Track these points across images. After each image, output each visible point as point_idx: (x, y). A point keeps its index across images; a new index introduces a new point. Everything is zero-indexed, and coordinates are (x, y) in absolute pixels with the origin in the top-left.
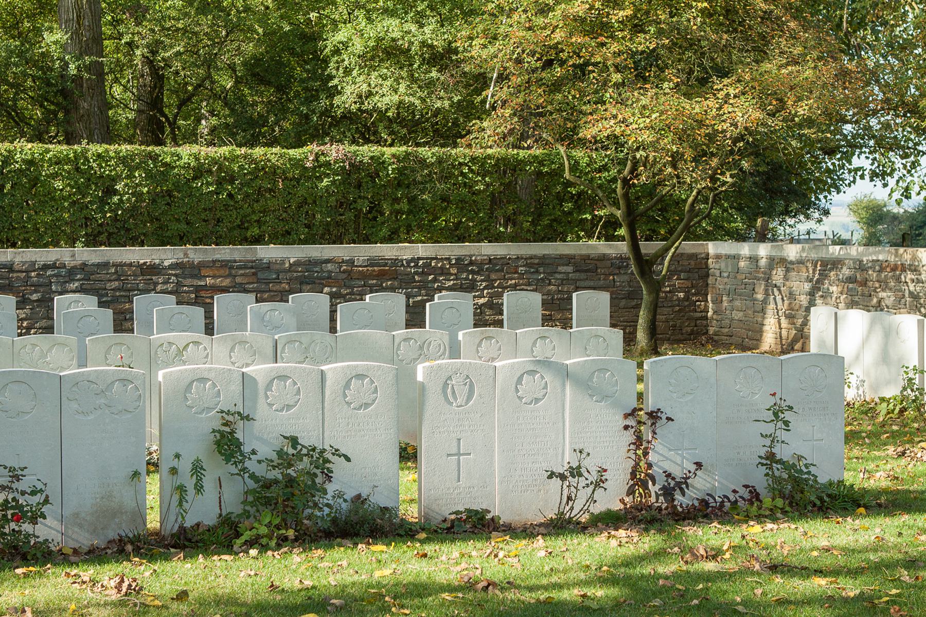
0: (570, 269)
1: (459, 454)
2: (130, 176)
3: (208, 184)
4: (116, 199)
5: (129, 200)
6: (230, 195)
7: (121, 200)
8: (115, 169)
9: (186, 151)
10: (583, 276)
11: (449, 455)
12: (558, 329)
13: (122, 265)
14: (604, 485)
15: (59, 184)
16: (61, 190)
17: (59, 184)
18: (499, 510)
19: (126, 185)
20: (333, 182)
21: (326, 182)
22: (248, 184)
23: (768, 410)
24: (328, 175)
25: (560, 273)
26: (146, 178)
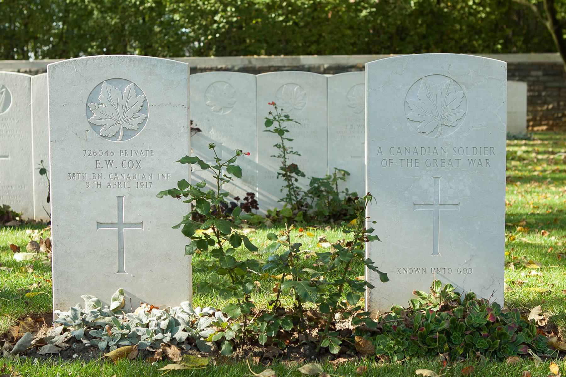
0: (540, 73)
1: (120, 224)
2: (224, 11)
3: (279, 15)
4: (215, 26)
5: (224, 27)
6: (296, 24)
7: (218, 27)
8: (214, 6)
10: (551, 79)
11: (99, 224)
12: (136, 56)
13: (99, 54)
14: (372, 234)
15: (177, 17)
16: (179, 21)
17: (177, 17)
19: (222, 16)
20: (370, 13)
21: (364, 13)
22: (309, 15)
23: (176, 227)
24: (366, 8)
25: (532, 76)
26: (235, 12)
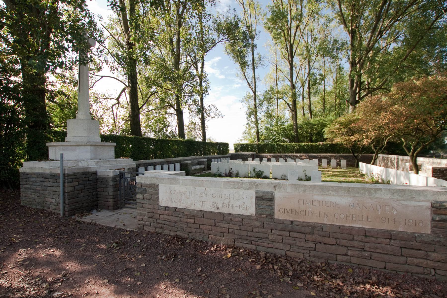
9: (303, 144)
18: (277, 177)
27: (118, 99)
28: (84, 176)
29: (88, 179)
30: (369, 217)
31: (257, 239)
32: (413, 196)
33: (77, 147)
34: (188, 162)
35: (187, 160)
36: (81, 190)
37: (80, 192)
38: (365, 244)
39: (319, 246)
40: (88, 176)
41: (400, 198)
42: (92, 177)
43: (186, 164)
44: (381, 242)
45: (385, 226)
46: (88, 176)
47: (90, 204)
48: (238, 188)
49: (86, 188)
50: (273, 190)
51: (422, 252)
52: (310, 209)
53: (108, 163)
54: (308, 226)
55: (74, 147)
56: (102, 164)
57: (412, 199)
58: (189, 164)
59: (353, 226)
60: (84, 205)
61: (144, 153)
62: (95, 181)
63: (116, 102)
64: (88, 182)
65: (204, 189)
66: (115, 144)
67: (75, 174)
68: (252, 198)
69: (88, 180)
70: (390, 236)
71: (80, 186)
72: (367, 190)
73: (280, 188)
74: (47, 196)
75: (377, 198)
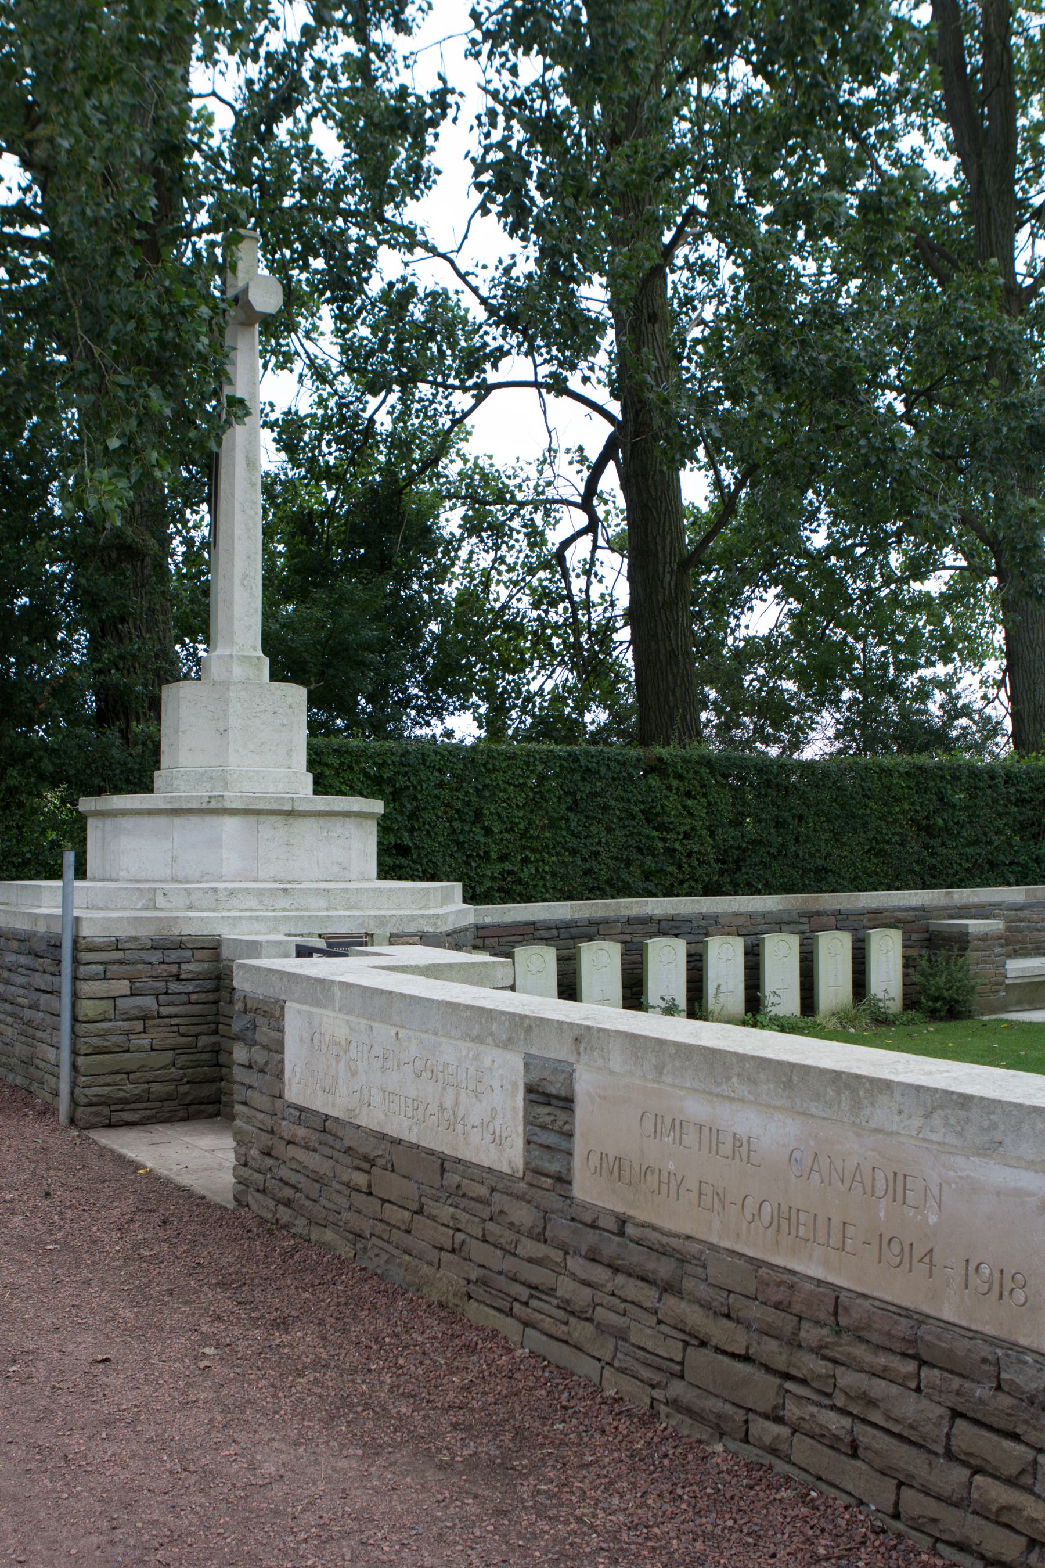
27: (586, 504)
28: (155, 957)
29: (174, 969)
30: (850, 1230)
31: (524, 1293)
32: (998, 1136)
33: (177, 821)
34: (975, 926)
35: (982, 912)
36: (144, 1018)
37: (139, 1026)
38: (840, 1371)
39: (698, 1357)
40: (173, 955)
41: (951, 1139)
42: (191, 967)
43: (961, 941)
44: (885, 1369)
45: (899, 1288)
46: (173, 955)
47: (184, 1089)
48: (478, 1039)
49: (165, 1011)
50: (572, 1059)
51: (1022, 1448)
52: (671, 1167)
53: (282, 902)
54: (664, 1252)
55: (162, 821)
56: (253, 903)
57: (991, 1149)
58: (984, 938)
59: (798, 1268)
60: (155, 1087)
61: (670, 852)
62: (209, 985)
63: (581, 519)
64: (174, 987)
65: (393, 1033)
66: (378, 806)
67: (116, 945)
68: (515, 1084)
69: (178, 978)
70: (917, 1346)
71: (139, 1001)
72: (847, 1086)
73: (593, 1049)
74: (39, 1034)
75: (877, 1131)
